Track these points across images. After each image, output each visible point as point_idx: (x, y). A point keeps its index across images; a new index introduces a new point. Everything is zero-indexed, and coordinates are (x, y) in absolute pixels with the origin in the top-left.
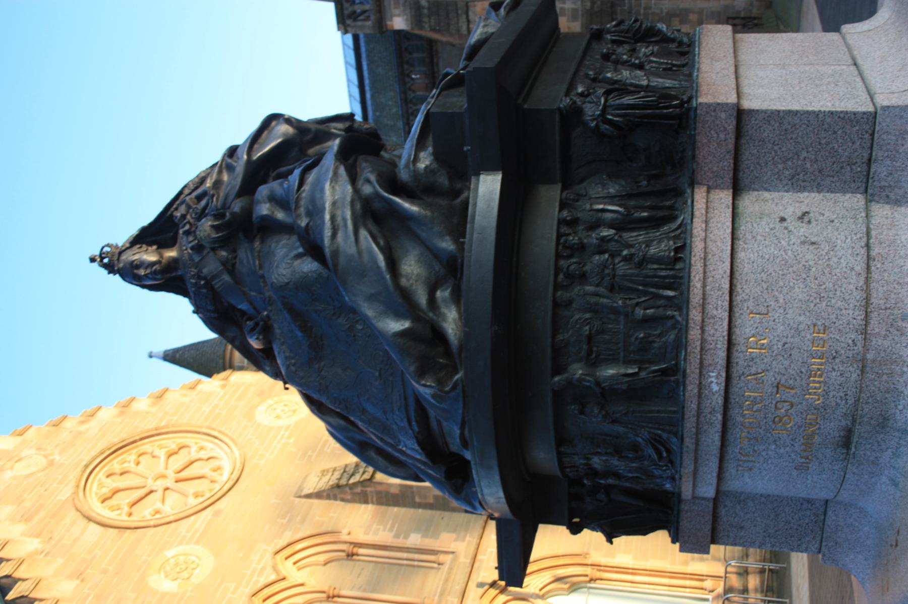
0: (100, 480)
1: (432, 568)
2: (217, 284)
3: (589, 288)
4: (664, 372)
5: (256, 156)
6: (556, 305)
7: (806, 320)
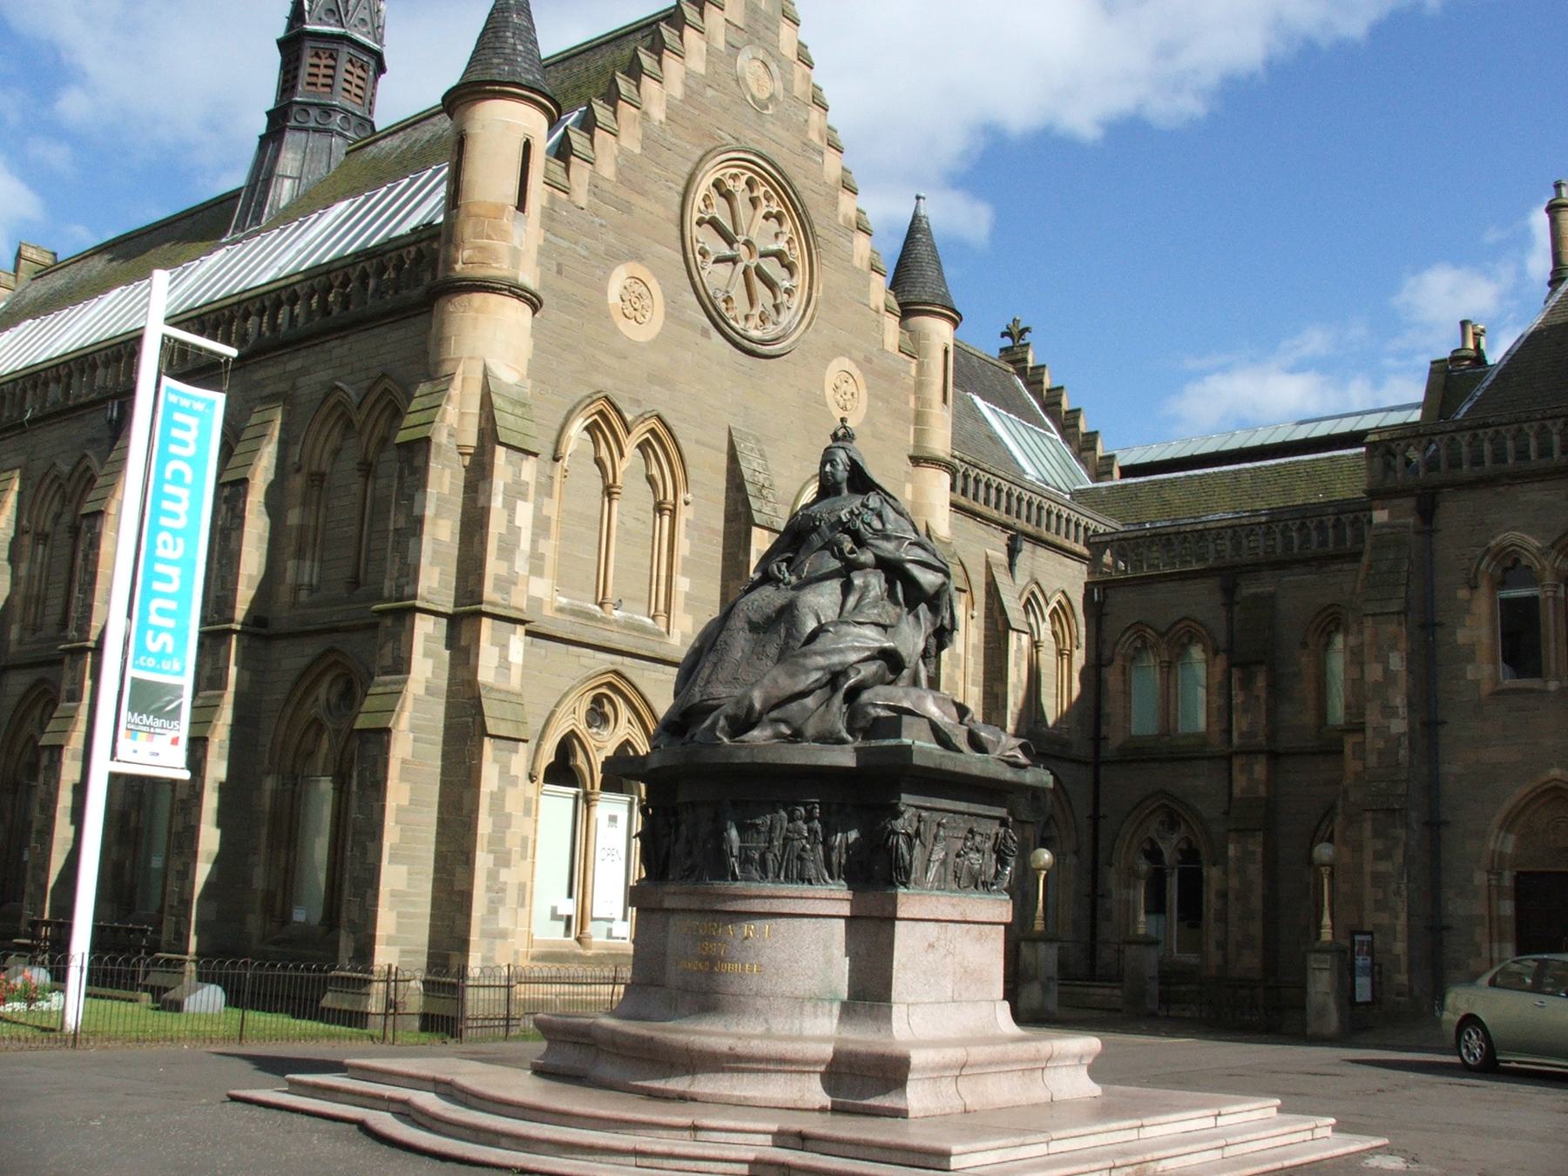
0: (743, 174)
3: (785, 824)
4: (734, 873)
5: (909, 566)
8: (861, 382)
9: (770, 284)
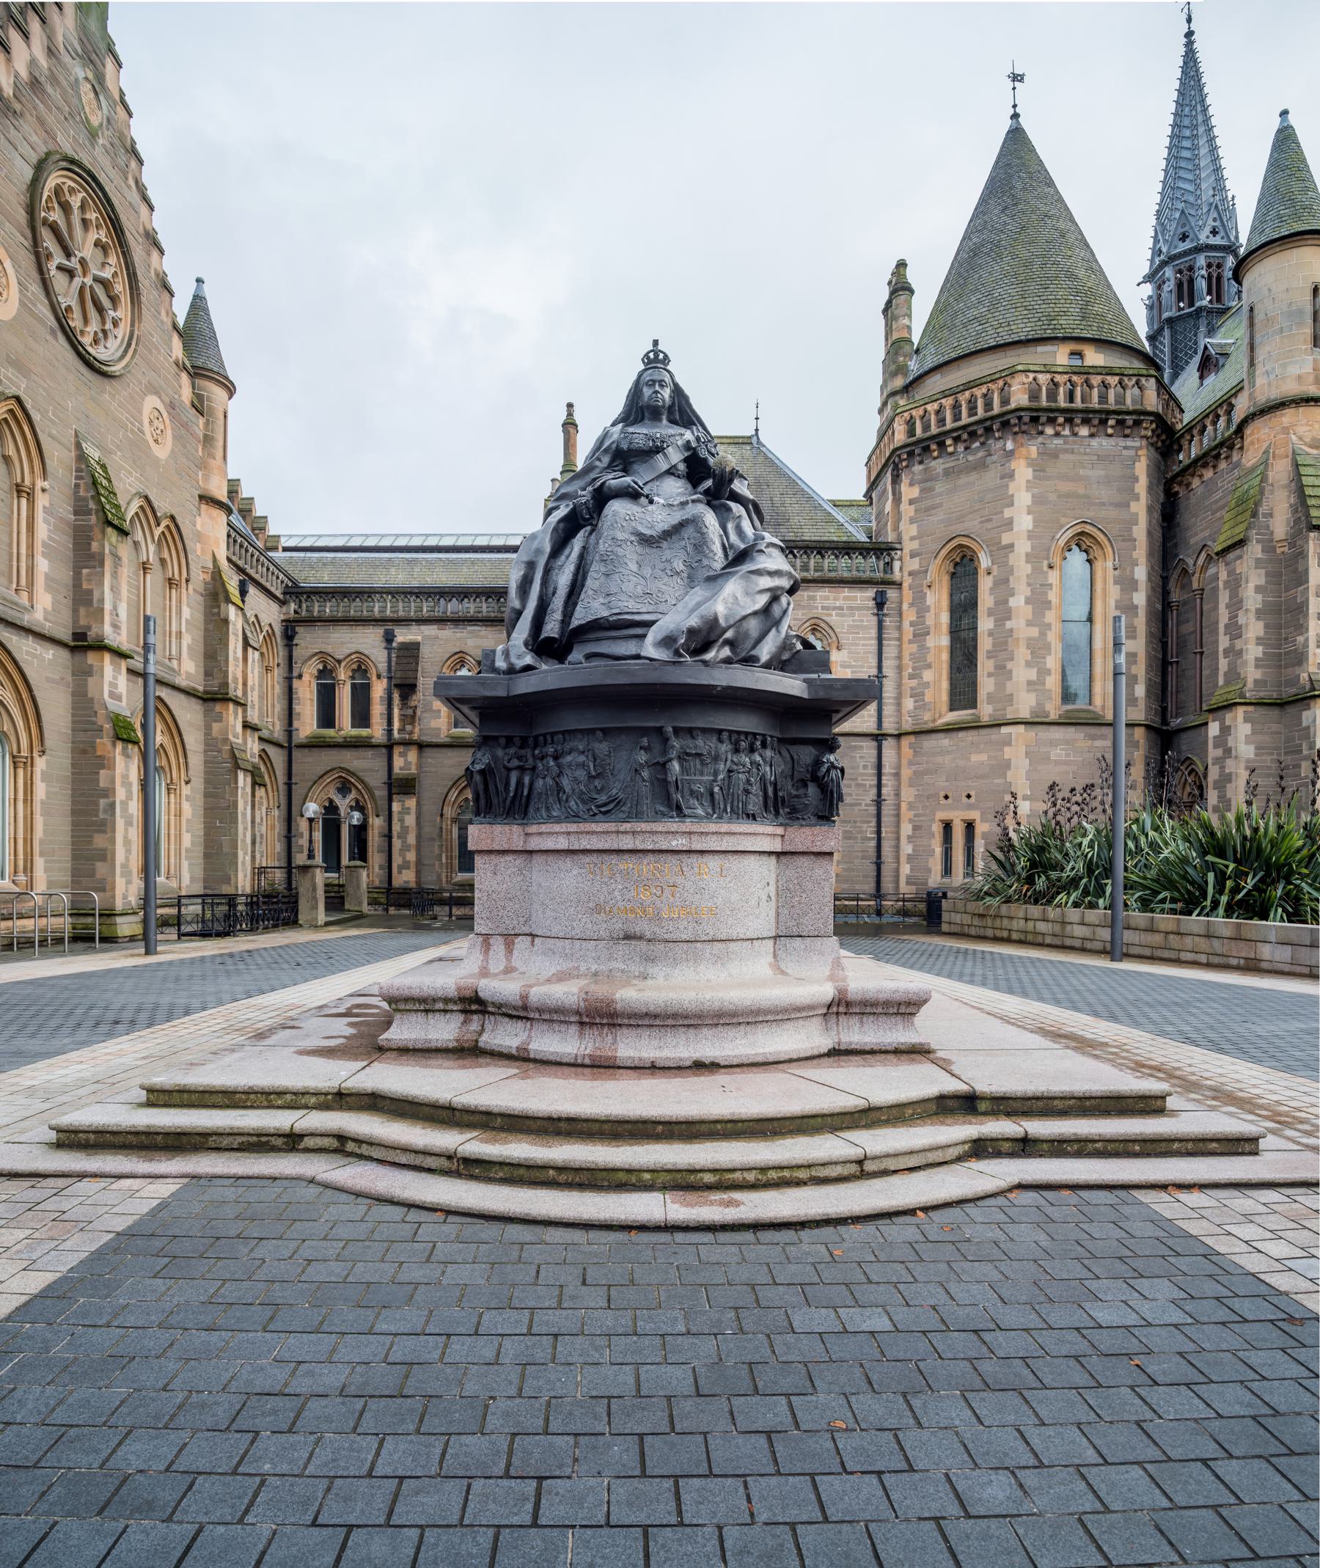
1: (11, 582)
2: (660, 456)
6: (720, 732)
7: (719, 901)
8: (167, 421)
9: (100, 310)
